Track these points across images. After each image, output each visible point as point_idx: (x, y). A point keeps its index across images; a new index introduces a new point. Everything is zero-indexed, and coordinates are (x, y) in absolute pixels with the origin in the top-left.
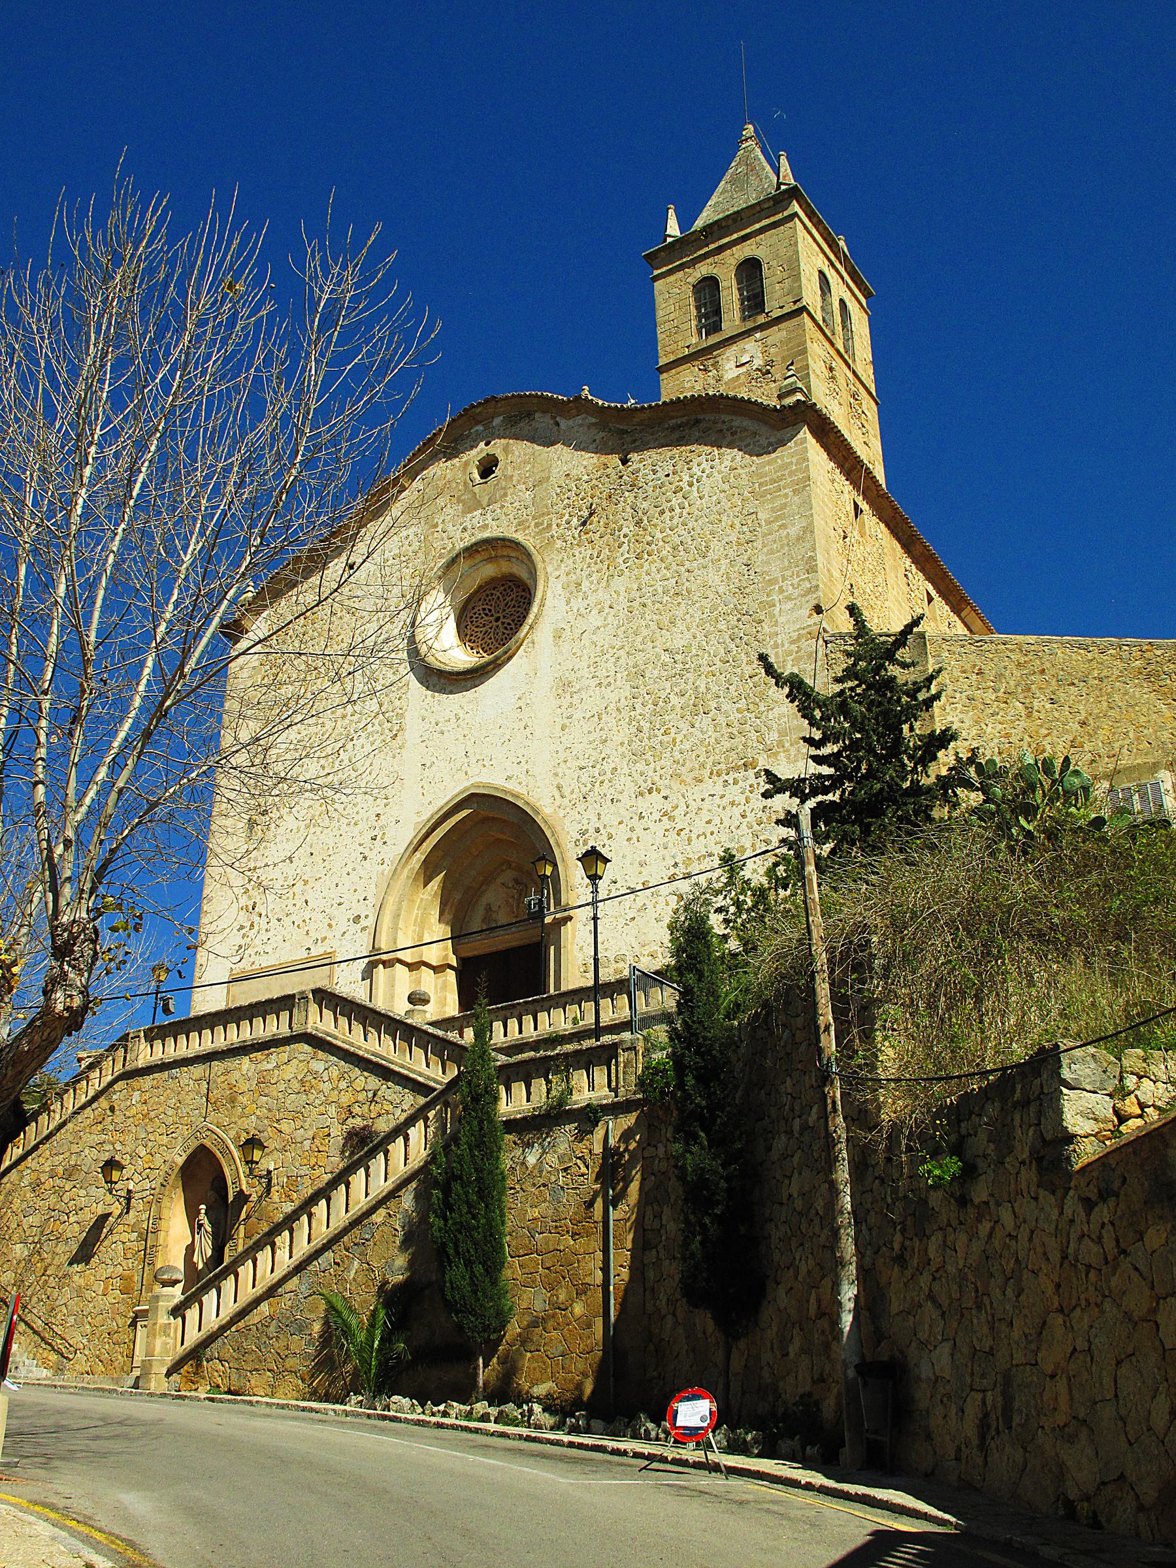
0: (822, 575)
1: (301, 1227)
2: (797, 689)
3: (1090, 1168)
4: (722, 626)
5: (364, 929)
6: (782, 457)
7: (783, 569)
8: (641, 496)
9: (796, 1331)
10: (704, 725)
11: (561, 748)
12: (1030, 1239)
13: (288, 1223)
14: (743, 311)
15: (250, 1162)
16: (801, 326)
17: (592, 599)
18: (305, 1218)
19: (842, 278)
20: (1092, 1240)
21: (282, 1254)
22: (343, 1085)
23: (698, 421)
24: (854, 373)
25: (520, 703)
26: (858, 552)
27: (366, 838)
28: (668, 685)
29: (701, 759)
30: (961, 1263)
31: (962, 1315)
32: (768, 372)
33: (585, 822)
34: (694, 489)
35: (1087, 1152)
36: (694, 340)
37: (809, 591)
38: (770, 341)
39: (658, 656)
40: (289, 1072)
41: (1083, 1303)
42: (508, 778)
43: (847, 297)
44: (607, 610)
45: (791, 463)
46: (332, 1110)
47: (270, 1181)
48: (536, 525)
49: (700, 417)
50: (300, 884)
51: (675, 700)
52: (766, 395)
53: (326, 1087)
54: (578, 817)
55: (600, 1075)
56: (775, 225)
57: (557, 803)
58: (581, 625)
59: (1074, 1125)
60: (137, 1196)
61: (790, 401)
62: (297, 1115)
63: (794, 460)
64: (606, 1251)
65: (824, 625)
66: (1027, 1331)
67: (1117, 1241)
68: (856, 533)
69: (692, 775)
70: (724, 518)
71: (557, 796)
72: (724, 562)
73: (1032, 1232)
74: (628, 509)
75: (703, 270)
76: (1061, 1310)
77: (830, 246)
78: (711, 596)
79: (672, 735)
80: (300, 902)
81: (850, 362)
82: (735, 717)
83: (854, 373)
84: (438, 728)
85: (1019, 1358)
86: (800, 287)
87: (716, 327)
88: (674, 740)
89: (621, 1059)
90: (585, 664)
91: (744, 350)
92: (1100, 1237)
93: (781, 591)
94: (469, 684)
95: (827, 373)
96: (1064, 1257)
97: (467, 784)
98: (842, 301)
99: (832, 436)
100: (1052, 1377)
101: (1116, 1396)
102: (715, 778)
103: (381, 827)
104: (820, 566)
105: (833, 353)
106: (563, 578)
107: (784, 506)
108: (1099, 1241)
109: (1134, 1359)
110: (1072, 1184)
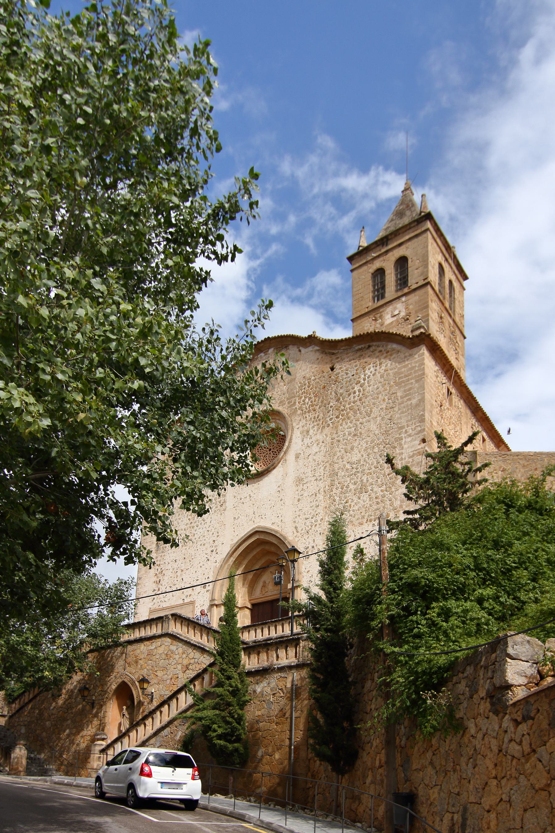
0: (427, 424)
1: (156, 717)
2: (405, 475)
3: (519, 703)
4: (376, 450)
5: (207, 591)
6: (411, 364)
7: (407, 421)
8: (340, 386)
9: (370, 773)
10: (365, 498)
11: (297, 510)
12: (483, 739)
13: (151, 713)
14: (397, 286)
15: (143, 689)
16: (427, 293)
17: (314, 439)
18: (158, 713)
19: (452, 268)
20: (517, 743)
21: (149, 728)
22: (184, 656)
23: (369, 347)
24: (454, 321)
25: (279, 489)
26: (448, 414)
27: (209, 551)
28: (348, 479)
29: (363, 514)
30: (447, 748)
31: (446, 774)
32: (408, 319)
33: (307, 543)
34: (366, 382)
35: (520, 693)
36: (370, 304)
37: (420, 432)
38: (410, 302)
39: (344, 466)
40: (161, 650)
41: (508, 777)
42: (273, 523)
43: (453, 278)
44: (321, 444)
45: (415, 366)
46: (179, 667)
47: (152, 696)
48: (289, 403)
49: (371, 344)
50: (179, 572)
51: (352, 487)
52: (406, 331)
53: (177, 657)
54: (304, 541)
55: (291, 652)
56: (417, 236)
57: (295, 535)
58: (308, 451)
59: (512, 679)
60: (96, 702)
61: (417, 333)
62: (165, 669)
63: (417, 365)
64: (291, 731)
65: (426, 448)
66: (477, 786)
67: (531, 745)
68: (447, 404)
69: (357, 522)
70: (380, 396)
71: (295, 532)
72: (379, 419)
73: (484, 735)
74: (333, 393)
75: (377, 264)
76: (496, 778)
77: (446, 249)
78: (372, 436)
79: (350, 503)
80: (179, 579)
81: (452, 315)
82: (380, 494)
83: (454, 321)
84: (241, 501)
85: (472, 799)
86: (427, 271)
87: (383, 296)
88: (350, 505)
89: (301, 645)
90: (310, 470)
91: (395, 309)
92: (521, 741)
93: (406, 432)
94: (256, 480)
95: (438, 320)
96: (500, 751)
97: (254, 526)
98: (450, 282)
99: (438, 352)
100: (488, 811)
101: (522, 828)
102: (369, 523)
103: (216, 546)
104: (427, 419)
105: (443, 308)
106: (301, 429)
107: (410, 389)
108: (520, 743)
109: (534, 810)
110: (508, 712)
